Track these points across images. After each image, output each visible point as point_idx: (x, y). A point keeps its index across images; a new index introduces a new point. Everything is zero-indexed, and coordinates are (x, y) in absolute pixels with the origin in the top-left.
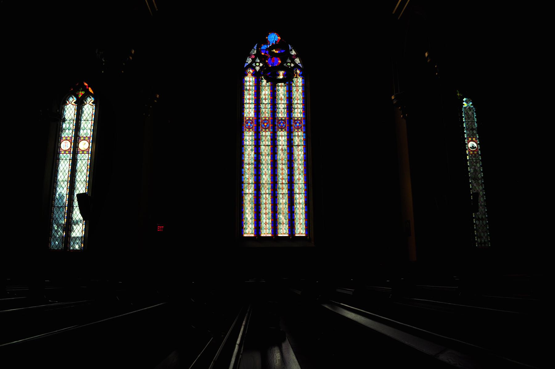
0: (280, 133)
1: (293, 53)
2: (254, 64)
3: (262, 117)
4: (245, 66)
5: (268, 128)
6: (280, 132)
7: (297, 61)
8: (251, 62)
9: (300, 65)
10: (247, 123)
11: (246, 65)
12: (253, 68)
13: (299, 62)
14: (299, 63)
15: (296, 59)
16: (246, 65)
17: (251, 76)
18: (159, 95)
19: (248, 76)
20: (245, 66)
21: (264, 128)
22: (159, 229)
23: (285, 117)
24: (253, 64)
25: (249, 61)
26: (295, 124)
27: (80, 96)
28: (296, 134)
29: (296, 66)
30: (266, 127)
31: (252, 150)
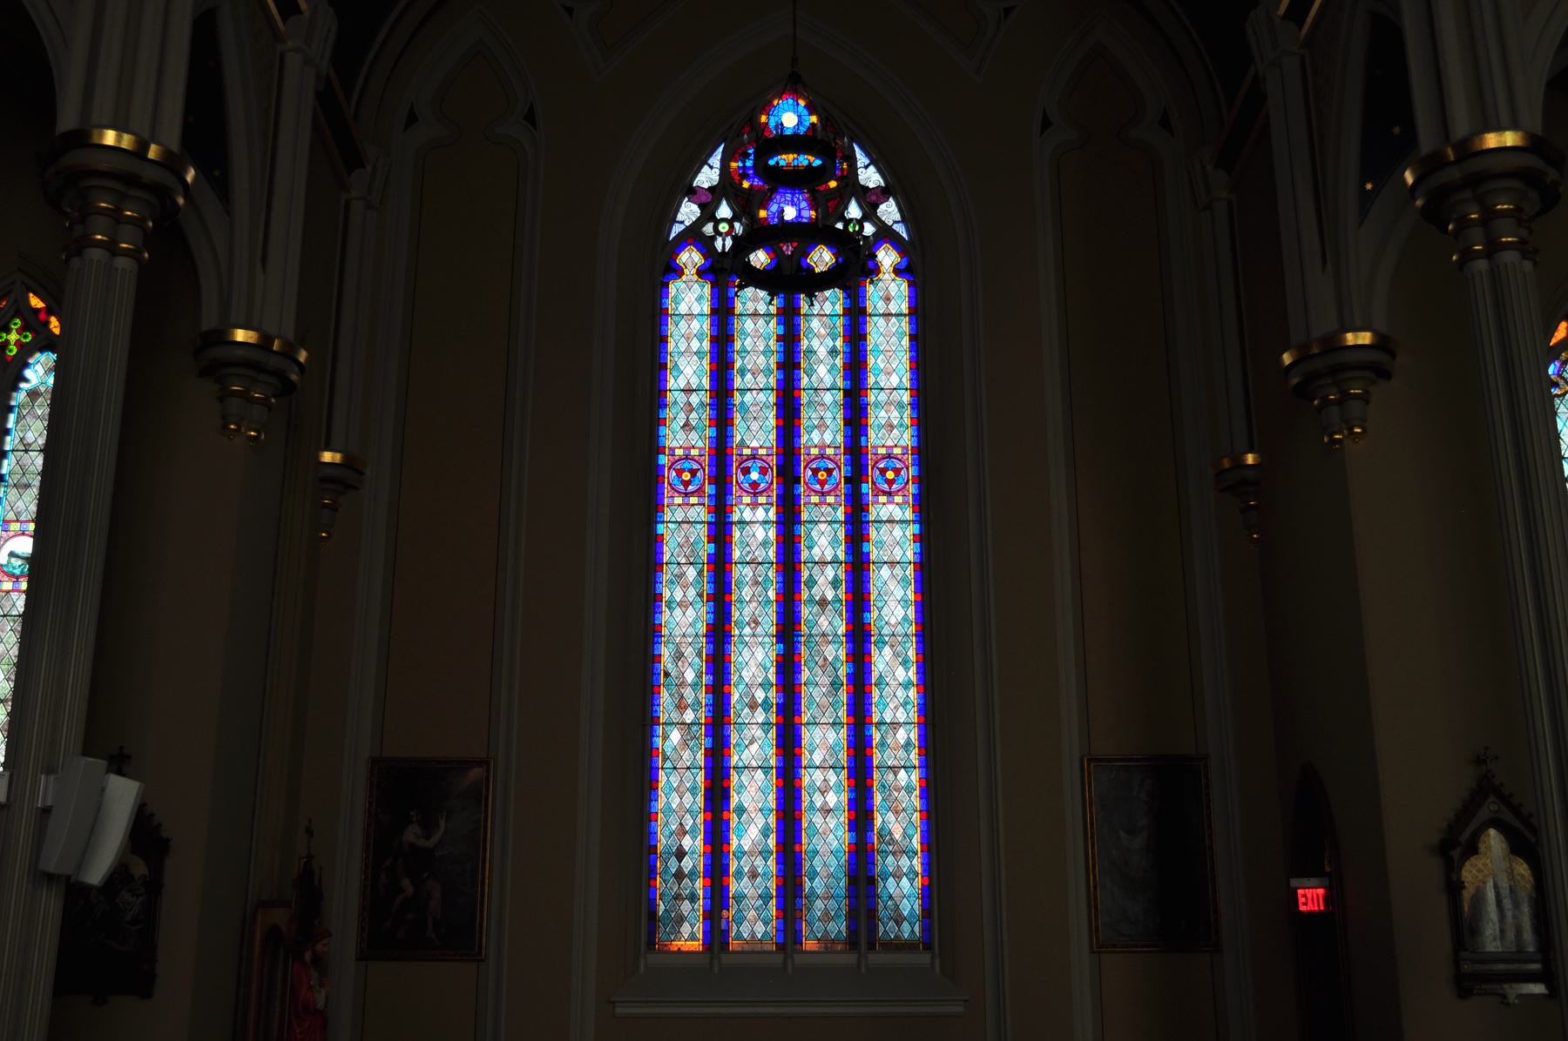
0: (741, 511)
1: (870, 177)
2: (708, 229)
3: (675, 444)
4: (673, 235)
5: (699, 492)
6: (884, 509)
7: (889, 211)
8: (698, 219)
9: (900, 229)
10: (746, 471)
11: (677, 229)
12: (705, 245)
13: (898, 217)
14: (895, 222)
15: (883, 207)
16: (677, 229)
17: (696, 277)
18: (308, 351)
19: (684, 278)
20: (673, 235)
21: (884, 493)
22: (1306, 904)
23: (902, 443)
24: (704, 229)
25: (689, 212)
26: (744, 475)
27: (11, 351)
28: (748, 515)
29: (885, 234)
30: (894, 486)
31: (835, 584)
